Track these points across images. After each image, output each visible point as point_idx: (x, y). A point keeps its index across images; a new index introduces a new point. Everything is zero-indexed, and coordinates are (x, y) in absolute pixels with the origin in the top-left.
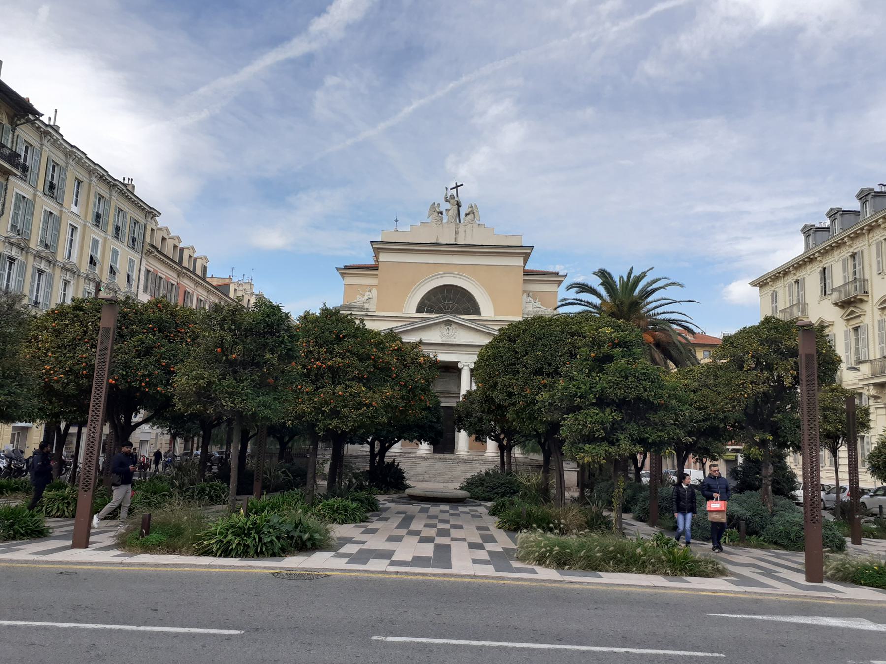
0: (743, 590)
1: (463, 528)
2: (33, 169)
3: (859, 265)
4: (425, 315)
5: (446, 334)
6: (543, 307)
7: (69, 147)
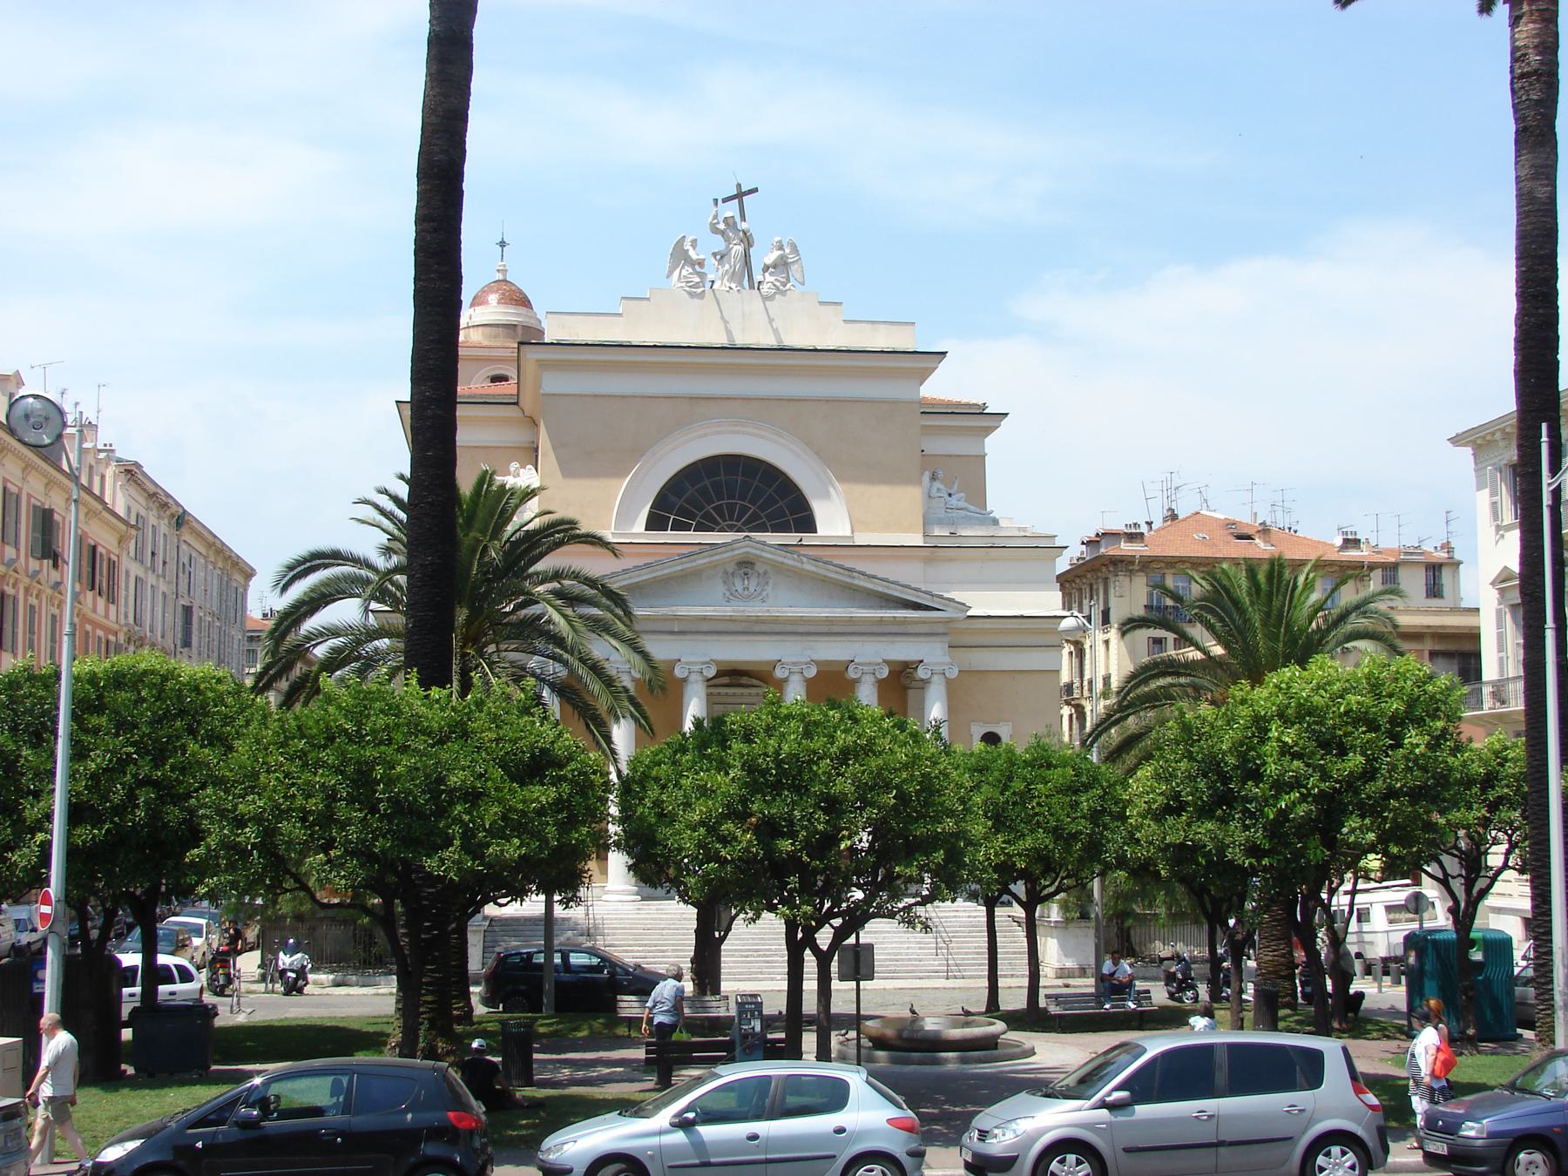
1: (1124, 1149)
4: (670, 536)
5: (740, 590)
6: (972, 508)
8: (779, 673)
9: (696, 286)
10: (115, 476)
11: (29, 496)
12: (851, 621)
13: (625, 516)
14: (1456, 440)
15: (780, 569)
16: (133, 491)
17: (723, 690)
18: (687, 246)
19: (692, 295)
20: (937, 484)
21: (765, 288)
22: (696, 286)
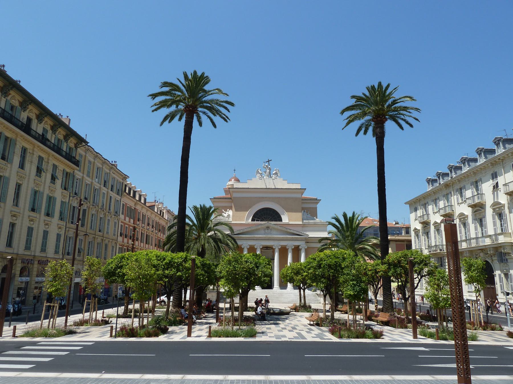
0: (49, 168)
2: (82, 164)
3: (430, 240)
4: (256, 222)
7: (95, 153)
8: (274, 247)
9: (261, 177)
10: (166, 212)
11: (147, 215)
12: (287, 238)
13: (248, 219)
14: (406, 203)
15: (274, 229)
16: (169, 214)
17: (265, 250)
18: (259, 170)
19: (260, 179)
20: (305, 213)
21: (273, 178)
22: (261, 177)
